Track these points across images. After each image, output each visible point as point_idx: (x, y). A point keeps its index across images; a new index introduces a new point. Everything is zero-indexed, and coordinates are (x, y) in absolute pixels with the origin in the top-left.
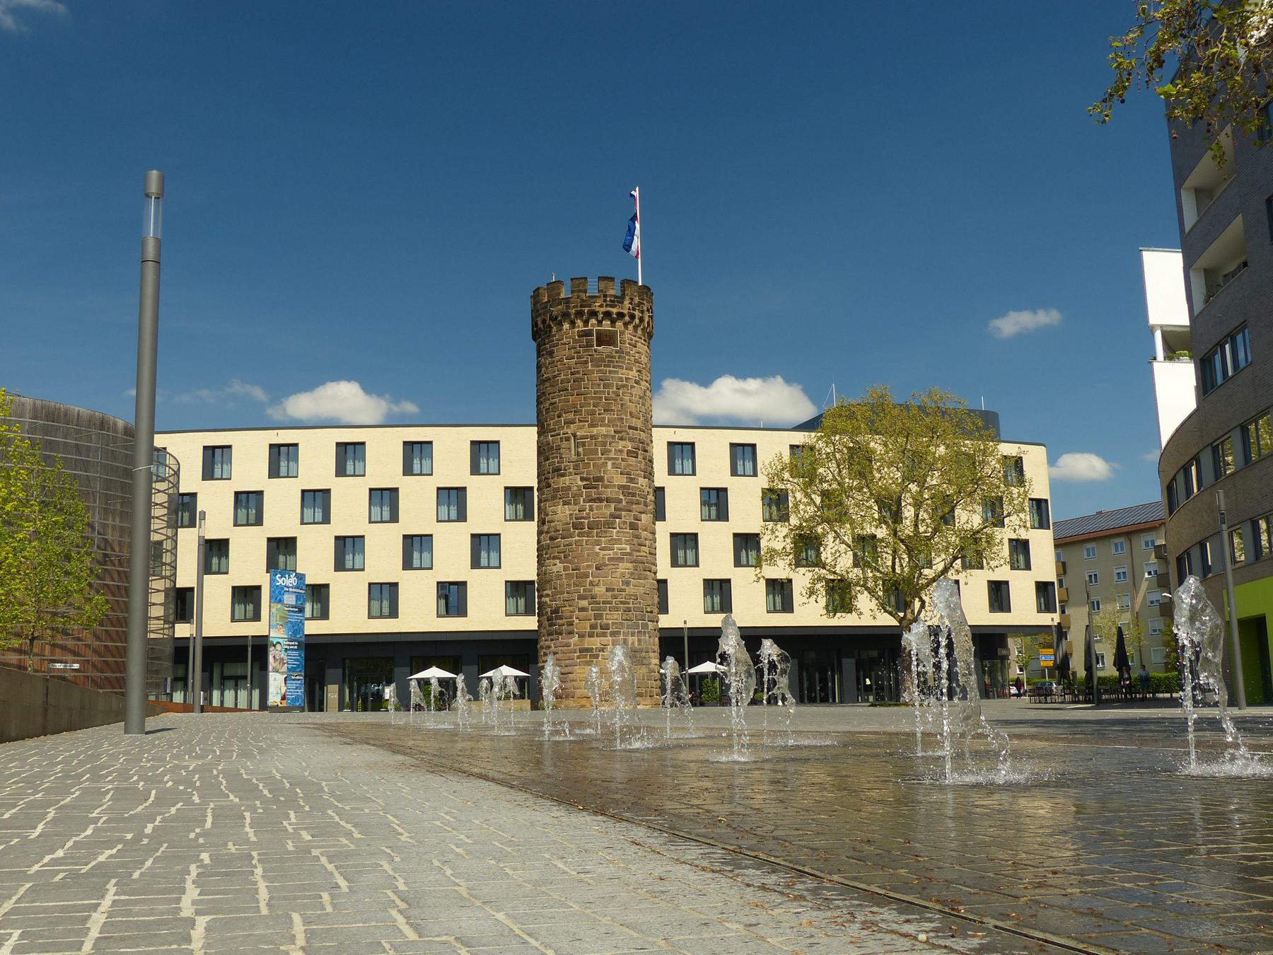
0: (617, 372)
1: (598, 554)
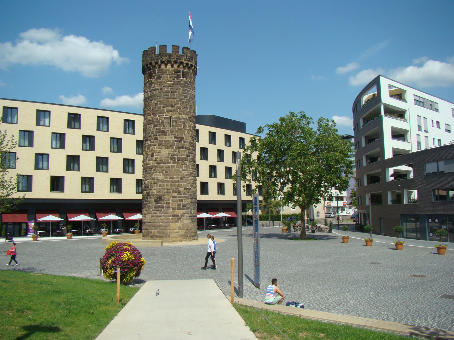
1: (181, 172)
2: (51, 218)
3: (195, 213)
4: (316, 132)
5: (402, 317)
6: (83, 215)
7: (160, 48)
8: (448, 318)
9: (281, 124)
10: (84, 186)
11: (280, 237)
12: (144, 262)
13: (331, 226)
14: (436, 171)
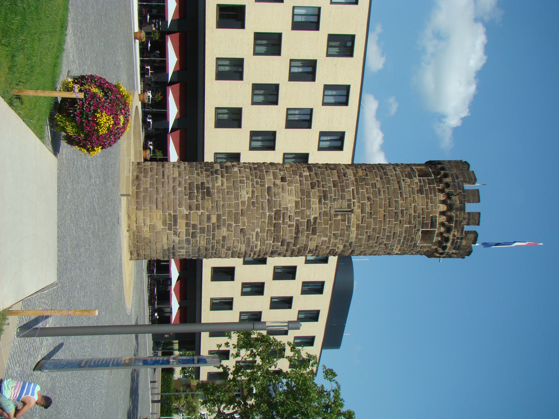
1: (253, 230)
7: (474, 190)
9: (342, 413)
10: (227, 63)
12: (93, 152)
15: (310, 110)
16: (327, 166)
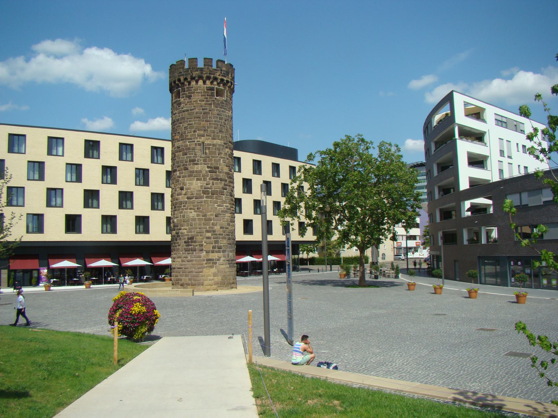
0: (225, 112)
1: (216, 208)
2: (66, 264)
3: (233, 257)
4: (377, 159)
5: (453, 380)
6: (103, 260)
8: (506, 380)
9: (335, 150)
10: (105, 226)
11: (335, 283)
13: (397, 271)
14: (519, 204)
15: (136, 170)
16: (173, 159)
